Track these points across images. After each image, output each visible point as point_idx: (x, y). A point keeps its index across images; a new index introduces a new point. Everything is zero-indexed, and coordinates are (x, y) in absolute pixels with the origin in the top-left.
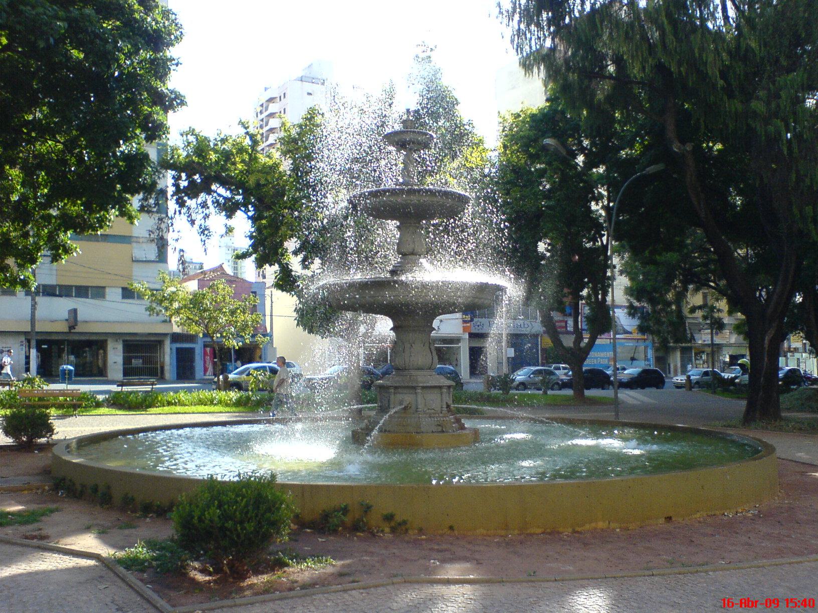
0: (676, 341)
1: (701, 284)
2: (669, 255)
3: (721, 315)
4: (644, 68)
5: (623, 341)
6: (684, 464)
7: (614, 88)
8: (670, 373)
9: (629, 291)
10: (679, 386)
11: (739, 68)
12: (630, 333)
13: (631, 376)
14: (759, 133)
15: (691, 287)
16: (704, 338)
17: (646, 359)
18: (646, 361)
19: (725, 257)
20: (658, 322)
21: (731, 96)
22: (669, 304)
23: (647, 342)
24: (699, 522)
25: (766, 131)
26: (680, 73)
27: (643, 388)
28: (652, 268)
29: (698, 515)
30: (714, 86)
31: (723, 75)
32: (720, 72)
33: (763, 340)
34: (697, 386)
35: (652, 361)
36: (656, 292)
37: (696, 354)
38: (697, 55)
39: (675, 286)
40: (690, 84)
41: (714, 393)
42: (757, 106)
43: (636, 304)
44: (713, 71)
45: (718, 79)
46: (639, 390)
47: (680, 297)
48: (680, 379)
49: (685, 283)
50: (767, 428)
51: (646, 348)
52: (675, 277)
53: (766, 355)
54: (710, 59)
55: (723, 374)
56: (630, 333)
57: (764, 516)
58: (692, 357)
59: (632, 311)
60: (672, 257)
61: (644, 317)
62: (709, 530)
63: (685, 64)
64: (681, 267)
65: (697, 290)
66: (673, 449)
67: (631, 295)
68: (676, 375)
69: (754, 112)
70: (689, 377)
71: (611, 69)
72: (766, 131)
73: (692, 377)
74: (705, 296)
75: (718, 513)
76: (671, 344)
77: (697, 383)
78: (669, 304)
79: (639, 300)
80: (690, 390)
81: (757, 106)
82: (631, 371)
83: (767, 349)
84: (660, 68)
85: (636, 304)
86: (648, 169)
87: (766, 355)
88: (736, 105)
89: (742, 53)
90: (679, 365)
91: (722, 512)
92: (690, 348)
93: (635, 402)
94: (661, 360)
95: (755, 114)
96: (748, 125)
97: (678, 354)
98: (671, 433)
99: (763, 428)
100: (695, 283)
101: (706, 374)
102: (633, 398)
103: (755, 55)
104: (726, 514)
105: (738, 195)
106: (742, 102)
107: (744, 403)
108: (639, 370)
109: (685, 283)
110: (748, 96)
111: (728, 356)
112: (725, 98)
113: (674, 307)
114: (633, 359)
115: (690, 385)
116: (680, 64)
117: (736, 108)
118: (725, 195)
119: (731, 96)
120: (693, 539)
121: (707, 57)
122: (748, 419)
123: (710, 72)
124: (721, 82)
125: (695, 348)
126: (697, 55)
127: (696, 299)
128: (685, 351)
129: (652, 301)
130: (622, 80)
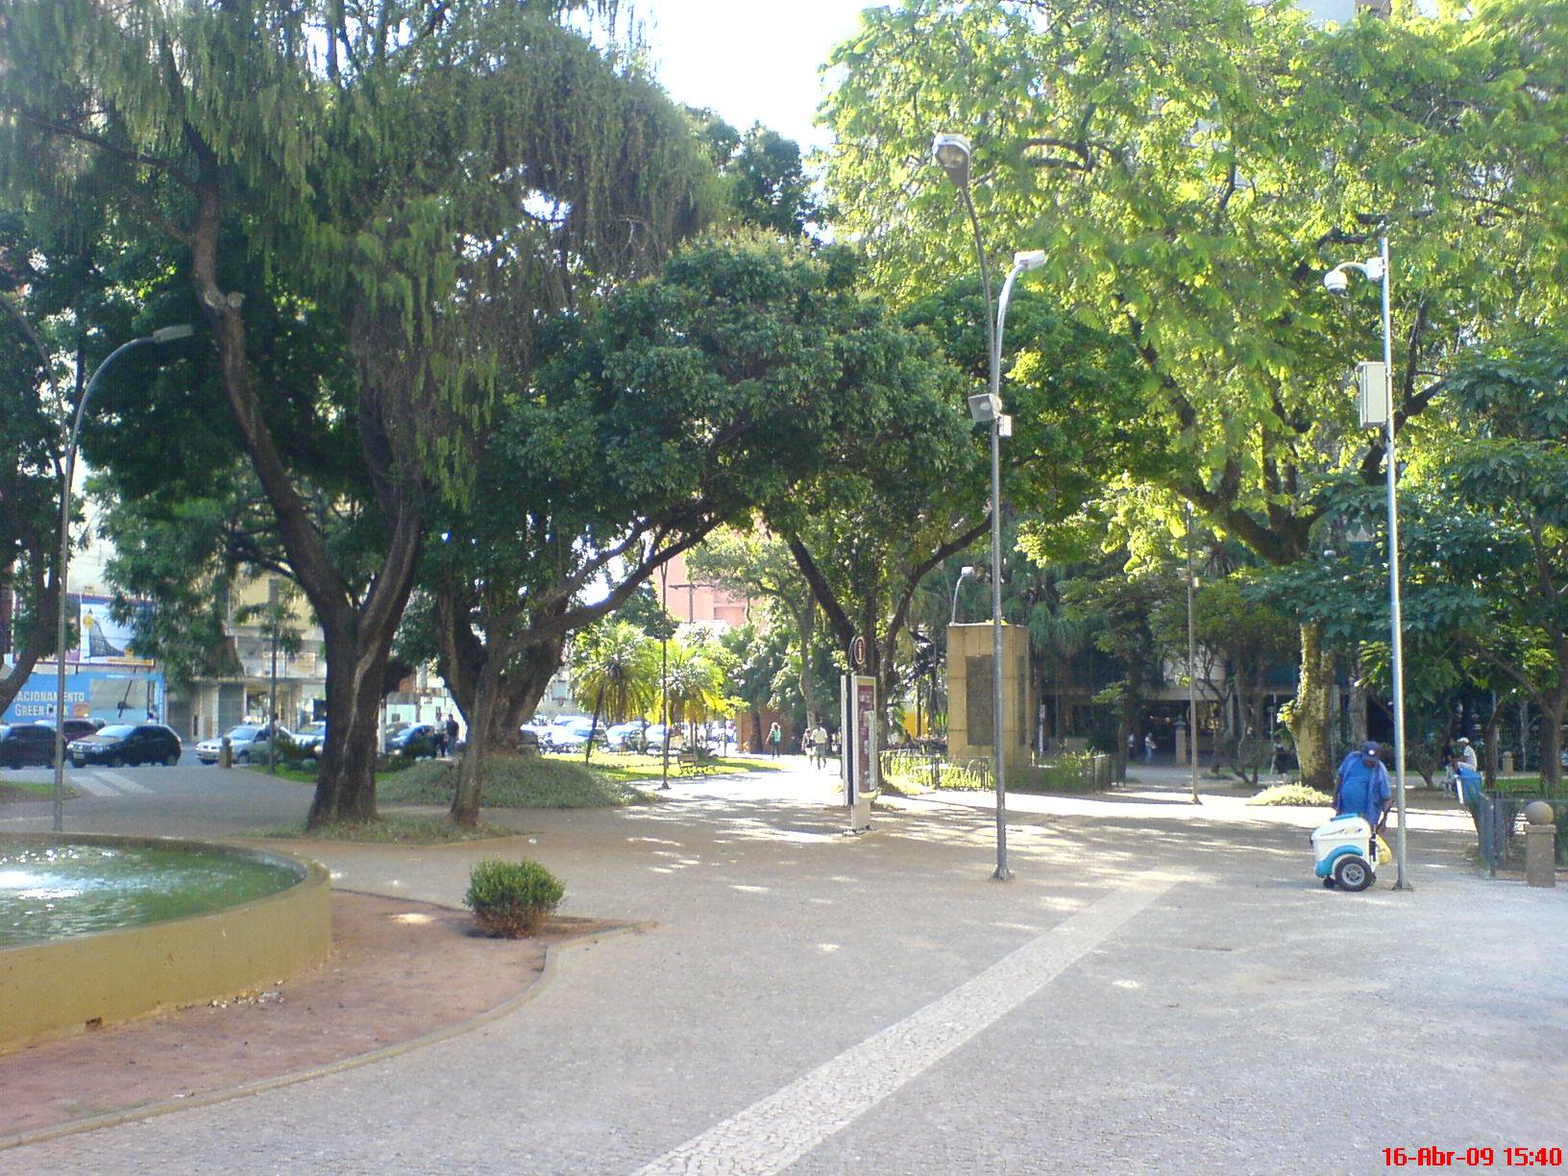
0: (209, 671)
1: (263, 564)
2: (201, 502)
3: (297, 625)
4: (1117, 155)
5: (105, 669)
6: (156, 911)
7: (100, 161)
8: (196, 733)
9: (113, 571)
10: (208, 760)
11: (346, 170)
12: (121, 654)
13: (112, 741)
14: (367, 293)
15: (243, 566)
16: (258, 669)
17: (151, 708)
18: (150, 709)
19: (287, 519)
20: (172, 634)
21: (324, 218)
22: (196, 600)
23: (153, 672)
24: (158, 1023)
25: (379, 291)
26: (231, 157)
27: (135, 763)
28: (161, 525)
29: (158, 1010)
30: (295, 193)
31: (314, 177)
32: (309, 170)
33: (352, 674)
34: (243, 758)
35: (162, 711)
36: (173, 576)
37: (249, 698)
38: (266, 130)
39: (213, 565)
40: (251, 183)
41: (273, 771)
42: (365, 241)
43: (129, 596)
44: (295, 166)
45: (303, 182)
46: (127, 768)
47: (222, 588)
48: (212, 745)
49: (232, 561)
50: (348, 837)
51: (151, 685)
52: (212, 548)
53: (355, 702)
54: (292, 143)
55: (294, 736)
56: (121, 654)
57: (284, 1001)
58: (242, 702)
59: (120, 611)
60: (202, 508)
61: (146, 624)
62: (172, 1038)
63: (242, 143)
64: (225, 530)
65: (255, 575)
66: (164, 882)
67: (121, 579)
68: (208, 736)
69: (362, 253)
70: (227, 742)
71: (99, 120)
72: (379, 291)
73: (233, 743)
74: (274, 589)
75: (199, 1002)
76: (197, 678)
77: (245, 753)
78: (196, 600)
79: (134, 588)
80: (228, 766)
81: (365, 241)
82: (114, 731)
83: (357, 691)
84: (192, 136)
85: (129, 596)
86: (158, 333)
87: (355, 702)
88: (331, 236)
89: (352, 141)
90: (215, 718)
91: (208, 1001)
92: (239, 687)
93: (108, 792)
94: (181, 710)
95: (363, 260)
96: (350, 275)
97: (215, 697)
98: (156, 852)
99: (340, 835)
100: (252, 561)
101: (262, 735)
102: (107, 783)
103: (372, 149)
104: (215, 1003)
105: (335, 401)
106: (343, 232)
107: (314, 788)
108: (129, 728)
109: (232, 561)
110: (354, 223)
111: (311, 702)
112: (312, 218)
113: (206, 607)
114: (122, 706)
115: (228, 757)
116: (232, 140)
117: (330, 244)
118: (306, 403)
119: (324, 218)
120: (134, 1059)
121: (285, 136)
122: (317, 819)
123: (289, 169)
124: (307, 190)
125: (251, 686)
126: (266, 130)
127: (254, 591)
128: (228, 691)
129: (163, 592)
130: (115, 149)
